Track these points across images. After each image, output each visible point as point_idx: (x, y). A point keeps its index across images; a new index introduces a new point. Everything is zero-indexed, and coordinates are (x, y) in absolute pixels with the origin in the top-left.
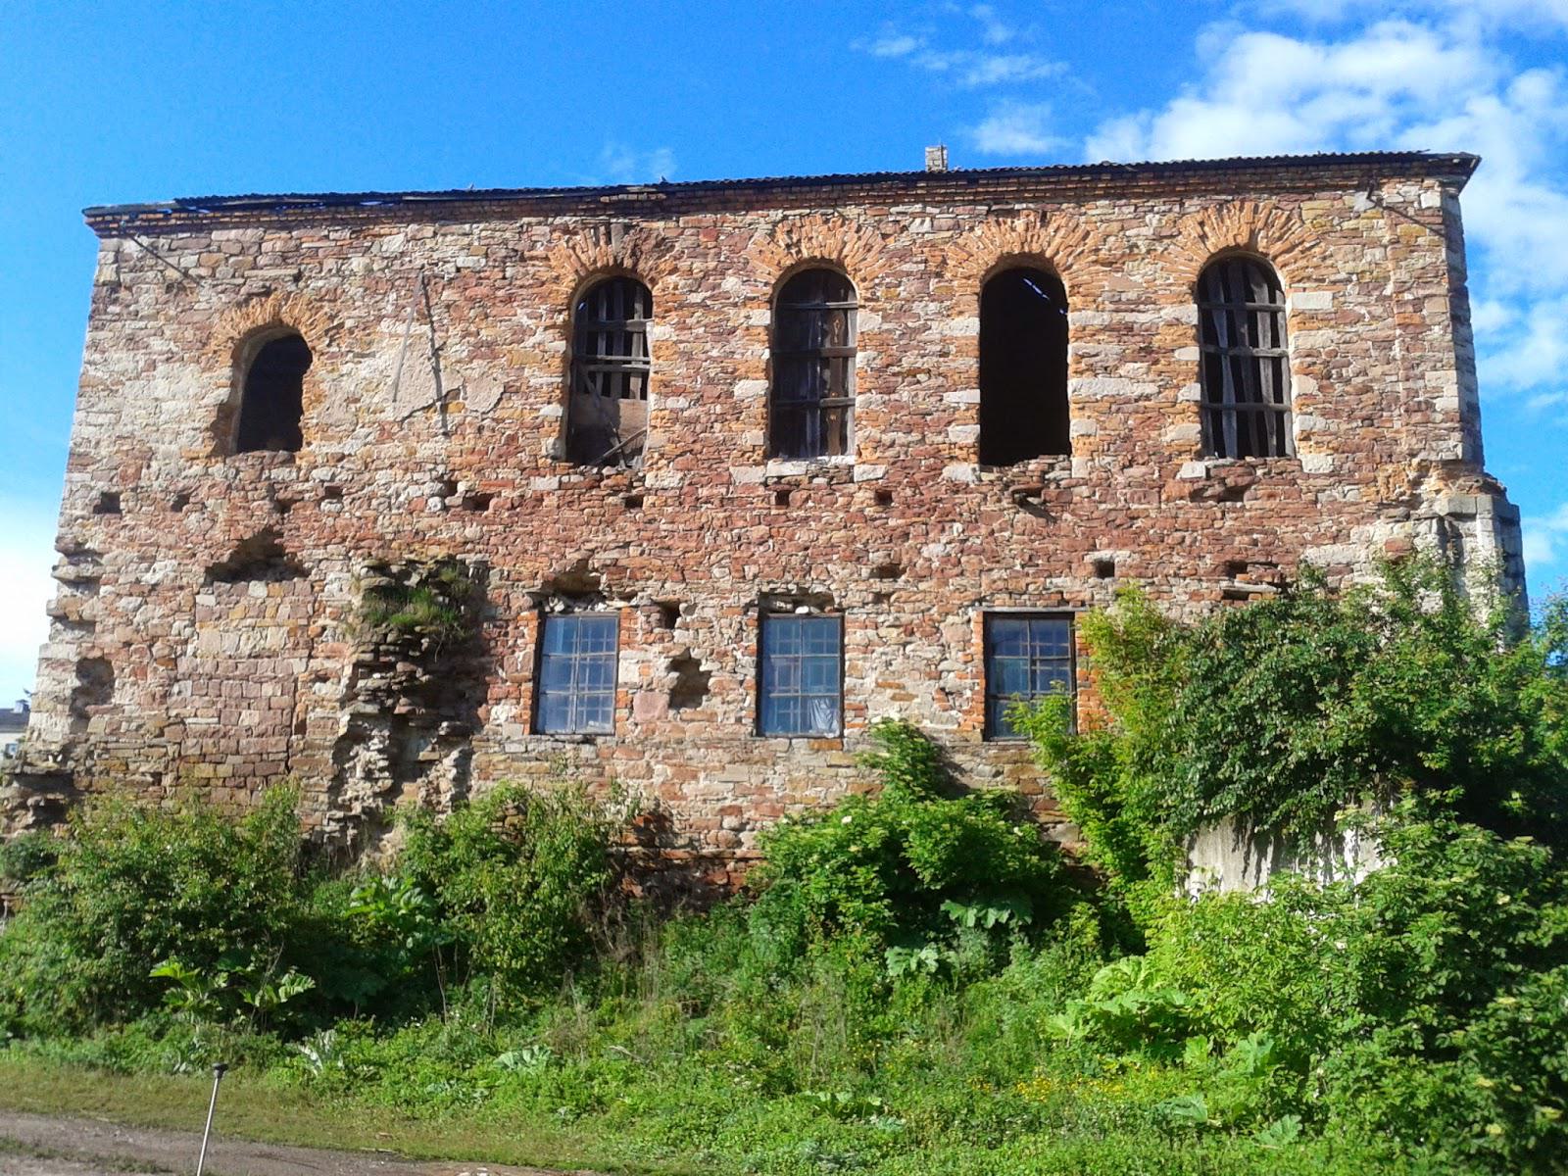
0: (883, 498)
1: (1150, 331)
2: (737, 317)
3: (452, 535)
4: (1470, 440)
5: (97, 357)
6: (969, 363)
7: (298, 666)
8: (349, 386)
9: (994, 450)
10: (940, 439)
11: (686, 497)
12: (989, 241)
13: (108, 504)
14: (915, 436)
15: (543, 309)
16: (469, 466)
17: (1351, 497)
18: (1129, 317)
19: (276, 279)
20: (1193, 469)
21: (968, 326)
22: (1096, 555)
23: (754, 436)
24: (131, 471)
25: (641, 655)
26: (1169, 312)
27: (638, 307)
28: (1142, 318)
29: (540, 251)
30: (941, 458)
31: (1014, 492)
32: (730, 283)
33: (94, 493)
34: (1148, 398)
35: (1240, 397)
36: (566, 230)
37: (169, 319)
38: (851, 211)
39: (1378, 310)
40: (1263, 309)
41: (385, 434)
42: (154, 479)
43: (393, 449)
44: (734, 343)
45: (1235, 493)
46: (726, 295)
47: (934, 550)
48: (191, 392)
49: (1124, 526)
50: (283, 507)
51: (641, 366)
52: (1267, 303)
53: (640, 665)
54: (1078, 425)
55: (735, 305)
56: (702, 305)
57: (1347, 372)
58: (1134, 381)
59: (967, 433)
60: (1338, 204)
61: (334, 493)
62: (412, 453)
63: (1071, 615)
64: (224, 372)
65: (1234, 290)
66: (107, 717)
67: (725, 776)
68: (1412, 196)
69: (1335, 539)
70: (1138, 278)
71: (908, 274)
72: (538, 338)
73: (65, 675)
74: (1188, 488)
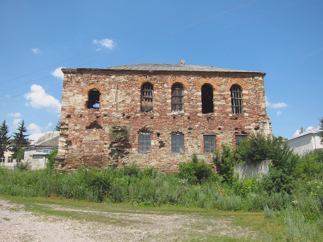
0: (189, 118)
1: (224, 95)
2: (166, 90)
3: (124, 123)
4: (99, 72)
5: (65, 93)
7: (102, 142)
8: (107, 99)
9: (204, 111)
10: (196, 110)
11: (160, 117)
12: (203, 81)
13: (69, 117)
14: (193, 109)
15: (137, 88)
16: (126, 112)
17: (251, 119)
18: (222, 93)
19: (94, 82)
20: (231, 115)
21: (200, 93)
22: (218, 127)
24: (72, 111)
25: (154, 141)
26: (227, 93)
27: (150, 88)
28: (223, 93)
29: (136, 79)
30: (197, 113)
31: (207, 118)
32: (165, 85)
33: (67, 115)
34: (224, 105)
37: (77, 87)
39: (254, 94)
40: (240, 107)
41: (113, 107)
42: (76, 112)
45: (236, 119)
47: (197, 126)
48: (82, 99)
49: (222, 123)
50: (97, 117)
51: (151, 97)
52: (240, 106)
53: (154, 142)
54: (215, 108)
55: (166, 89)
56: (161, 89)
57: (250, 102)
58: (223, 102)
59: (200, 109)
60: (249, 79)
61: (105, 115)
63: (215, 136)
64: (87, 96)
65: (236, 89)
66: (71, 150)
67: (168, 159)
68: (258, 78)
69: (249, 125)
70: (223, 88)
71: (191, 85)
72: (136, 92)
73: (64, 143)
74: (230, 118)
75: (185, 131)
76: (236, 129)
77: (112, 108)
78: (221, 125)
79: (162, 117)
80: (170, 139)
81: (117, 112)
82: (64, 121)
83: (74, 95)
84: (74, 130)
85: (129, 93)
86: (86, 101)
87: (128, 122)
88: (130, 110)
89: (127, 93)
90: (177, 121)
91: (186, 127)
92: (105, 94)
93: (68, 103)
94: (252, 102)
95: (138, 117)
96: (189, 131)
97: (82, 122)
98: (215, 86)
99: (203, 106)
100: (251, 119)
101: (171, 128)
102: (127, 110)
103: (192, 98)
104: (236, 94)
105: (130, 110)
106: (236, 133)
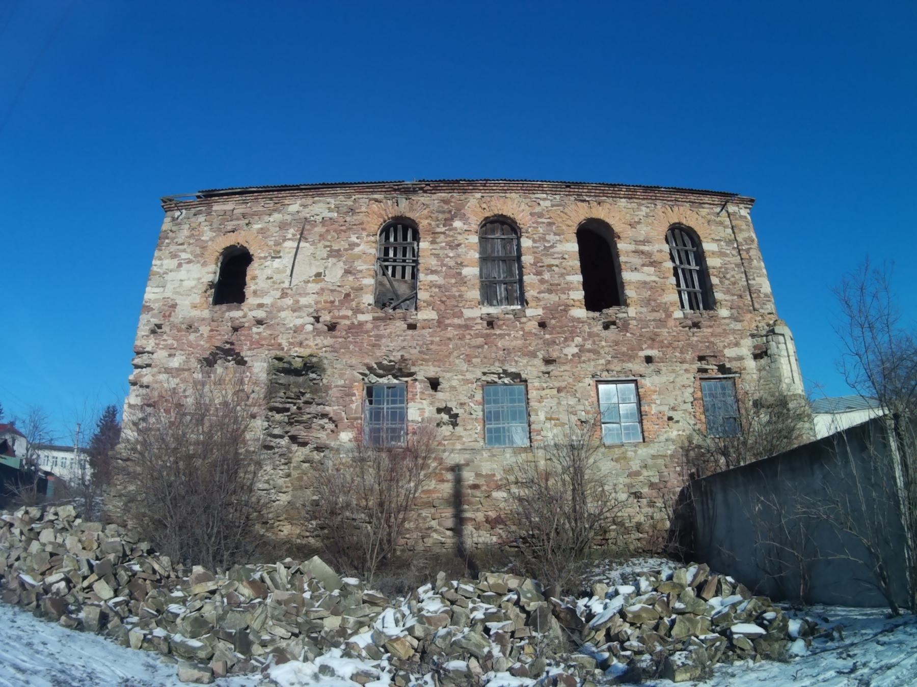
0: (542, 325)
3: (316, 345)
6: (575, 263)
8: (269, 272)
11: (441, 323)
21: (573, 247)
23: (475, 294)
24: (167, 314)
30: (567, 307)
32: (457, 224)
35: (687, 286)
36: (376, 200)
37: (189, 244)
38: (513, 195)
41: (284, 295)
43: (289, 301)
44: (461, 250)
46: (456, 229)
47: (572, 350)
49: (653, 340)
54: (630, 292)
55: (460, 234)
56: (444, 233)
58: (648, 274)
59: (579, 295)
61: (260, 322)
62: (297, 302)
75: (531, 369)
76: (701, 358)
77: (282, 297)
78: (651, 347)
79: (447, 322)
80: (479, 397)
81: (294, 311)
82: (145, 342)
83: (180, 265)
84: (168, 371)
85: (339, 250)
86: (211, 285)
87: (329, 341)
88: (337, 303)
89: (331, 251)
90: (501, 336)
91: (533, 355)
92: (265, 258)
93: (162, 289)
94: (733, 276)
95: (361, 324)
96: (544, 368)
97: (190, 345)
98: (617, 225)
99: (586, 285)
100: (739, 326)
101: (478, 360)
102: (326, 302)
103: (548, 261)
104: (683, 255)
105: (337, 303)
106: (701, 370)
